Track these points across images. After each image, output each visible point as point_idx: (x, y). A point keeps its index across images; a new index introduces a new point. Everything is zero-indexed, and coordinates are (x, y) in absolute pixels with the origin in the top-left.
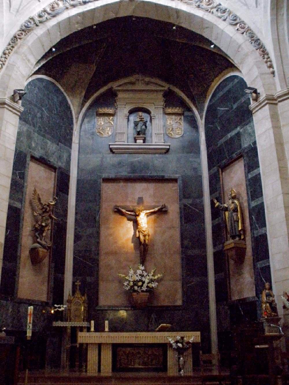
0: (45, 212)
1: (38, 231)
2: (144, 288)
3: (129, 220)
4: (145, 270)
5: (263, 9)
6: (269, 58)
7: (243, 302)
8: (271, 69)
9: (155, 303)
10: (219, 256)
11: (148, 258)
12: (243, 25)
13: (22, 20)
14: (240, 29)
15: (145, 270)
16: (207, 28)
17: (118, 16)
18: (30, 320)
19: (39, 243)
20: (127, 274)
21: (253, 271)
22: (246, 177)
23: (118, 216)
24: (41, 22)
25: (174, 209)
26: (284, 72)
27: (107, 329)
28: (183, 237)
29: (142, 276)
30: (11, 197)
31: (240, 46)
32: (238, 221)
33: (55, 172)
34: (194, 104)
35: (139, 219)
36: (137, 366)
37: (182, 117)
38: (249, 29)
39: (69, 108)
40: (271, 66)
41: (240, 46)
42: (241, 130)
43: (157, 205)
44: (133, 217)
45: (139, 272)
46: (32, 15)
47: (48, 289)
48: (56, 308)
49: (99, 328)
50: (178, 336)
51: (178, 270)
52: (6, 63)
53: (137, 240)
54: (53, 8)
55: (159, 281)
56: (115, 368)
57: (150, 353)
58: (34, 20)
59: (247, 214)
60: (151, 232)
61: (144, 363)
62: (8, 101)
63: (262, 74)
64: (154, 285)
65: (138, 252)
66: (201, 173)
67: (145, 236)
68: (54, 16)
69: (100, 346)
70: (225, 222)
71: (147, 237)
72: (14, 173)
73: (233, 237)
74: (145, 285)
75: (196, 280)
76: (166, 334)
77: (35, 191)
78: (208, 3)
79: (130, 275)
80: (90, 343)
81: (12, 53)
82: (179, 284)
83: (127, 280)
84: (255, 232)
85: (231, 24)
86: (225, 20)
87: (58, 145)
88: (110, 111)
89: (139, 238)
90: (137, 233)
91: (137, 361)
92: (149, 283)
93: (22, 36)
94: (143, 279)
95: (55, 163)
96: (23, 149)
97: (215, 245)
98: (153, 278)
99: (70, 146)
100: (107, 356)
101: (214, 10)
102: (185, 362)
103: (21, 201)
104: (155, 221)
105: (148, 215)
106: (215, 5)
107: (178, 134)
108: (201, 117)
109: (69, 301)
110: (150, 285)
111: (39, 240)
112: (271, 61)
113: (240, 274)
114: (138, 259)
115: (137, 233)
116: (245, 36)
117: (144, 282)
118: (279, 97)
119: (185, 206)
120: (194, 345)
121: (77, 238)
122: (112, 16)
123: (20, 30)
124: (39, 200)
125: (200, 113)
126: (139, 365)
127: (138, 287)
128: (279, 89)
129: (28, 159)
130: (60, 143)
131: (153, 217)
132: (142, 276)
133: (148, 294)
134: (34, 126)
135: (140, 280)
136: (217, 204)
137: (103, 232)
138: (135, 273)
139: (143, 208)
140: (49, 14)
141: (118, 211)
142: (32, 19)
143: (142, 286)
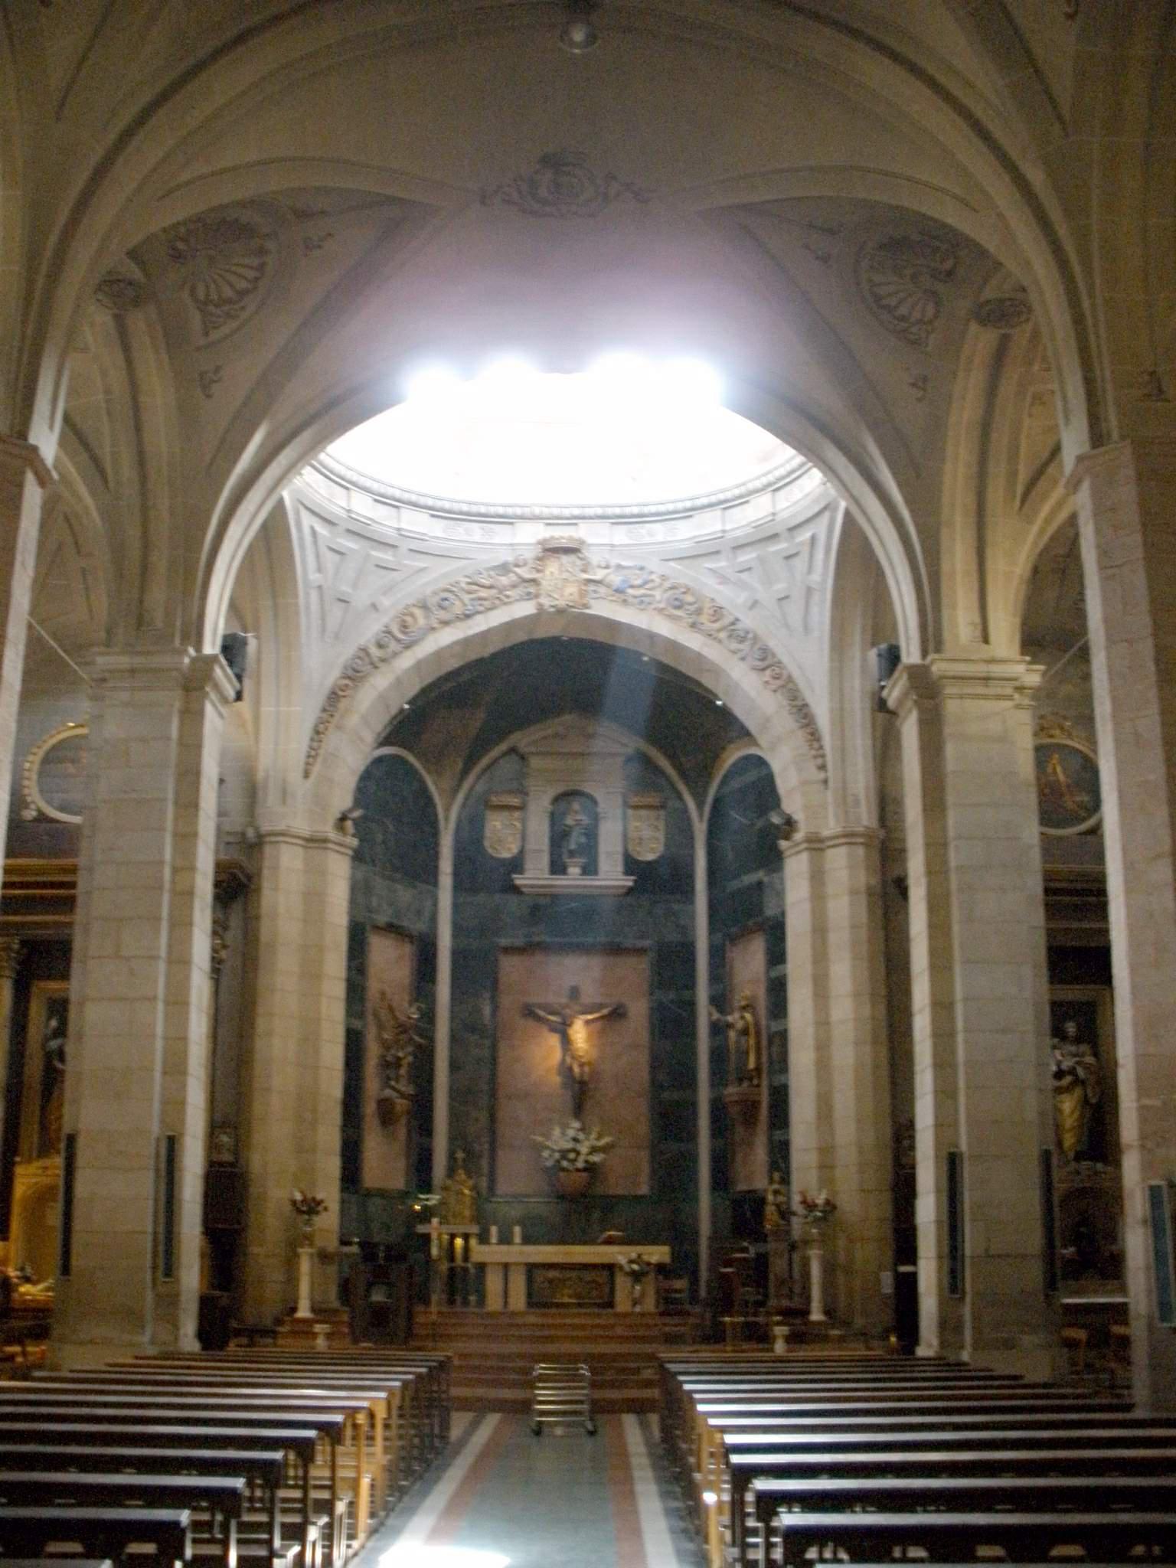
0: (405, 1032)
1: (389, 1066)
2: (580, 1164)
3: (553, 1030)
4: (582, 1130)
9: (600, 1190)
13: (347, 652)
14: (772, 681)
15: (582, 1130)
16: (708, 671)
18: (706, 1351)
20: (547, 1135)
23: (531, 1023)
24: (383, 660)
25: (639, 1009)
29: (575, 1140)
31: (768, 720)
32: (747, 1053)
33: (412, 942)
34: (687, 782)
36: (566, 1300)
40: (822, 767)
41: (768, 720)
42: (766, 879)
43: (608, 1001)
44: (559, 1027)
45: (571, 1133)
46: (362, 642)
49: (505, 1239)
50: (633, 1251)
51: (643, 1129)
52: (321, 752)
53: (566, 1071)
54: (404, 627)
56: (531, 1304)
59: (764, 1043)
61: (578, 1296)
63: (805, 783)
64: (596, 1158)
67: (582, 1065)
68: (408, 647)
69: (506, 1267)
74: (581, 1158)
78: (715, 618)
79: (554, 1138)
80: (491, 1263)
81: (331, 727)
82: (644, 1155)
83: (548, 1148)
85: (754, 669)
86: (743, 659)
87: (415, 887)
88: (515, 801)
89: (570, 1069)
92: (588, 1155)
94: (579, 1147)
97: (713, 1085)
100: (518, 1284)
101: (723, 635)
103: (361, 1015)
104: (602, 1033)
105: (587, 1022)
107: (652, 850)
108: (701, 816)
111: (393, 1083)
112: (823, 756)
113: (750, 1145)
120: (661, 1268)
121: (454, 1066)
122: (521, 637)
125: (700, 805)
128: (832, 822)
129: (368, 928)
132: (575, 1140)
135: (574, 1150)
136: (716, 1016)
137: (504, 1053)
138: (563, 1134)
141: (529, 1012)
142: (364, 650)
143: (575, 1160)
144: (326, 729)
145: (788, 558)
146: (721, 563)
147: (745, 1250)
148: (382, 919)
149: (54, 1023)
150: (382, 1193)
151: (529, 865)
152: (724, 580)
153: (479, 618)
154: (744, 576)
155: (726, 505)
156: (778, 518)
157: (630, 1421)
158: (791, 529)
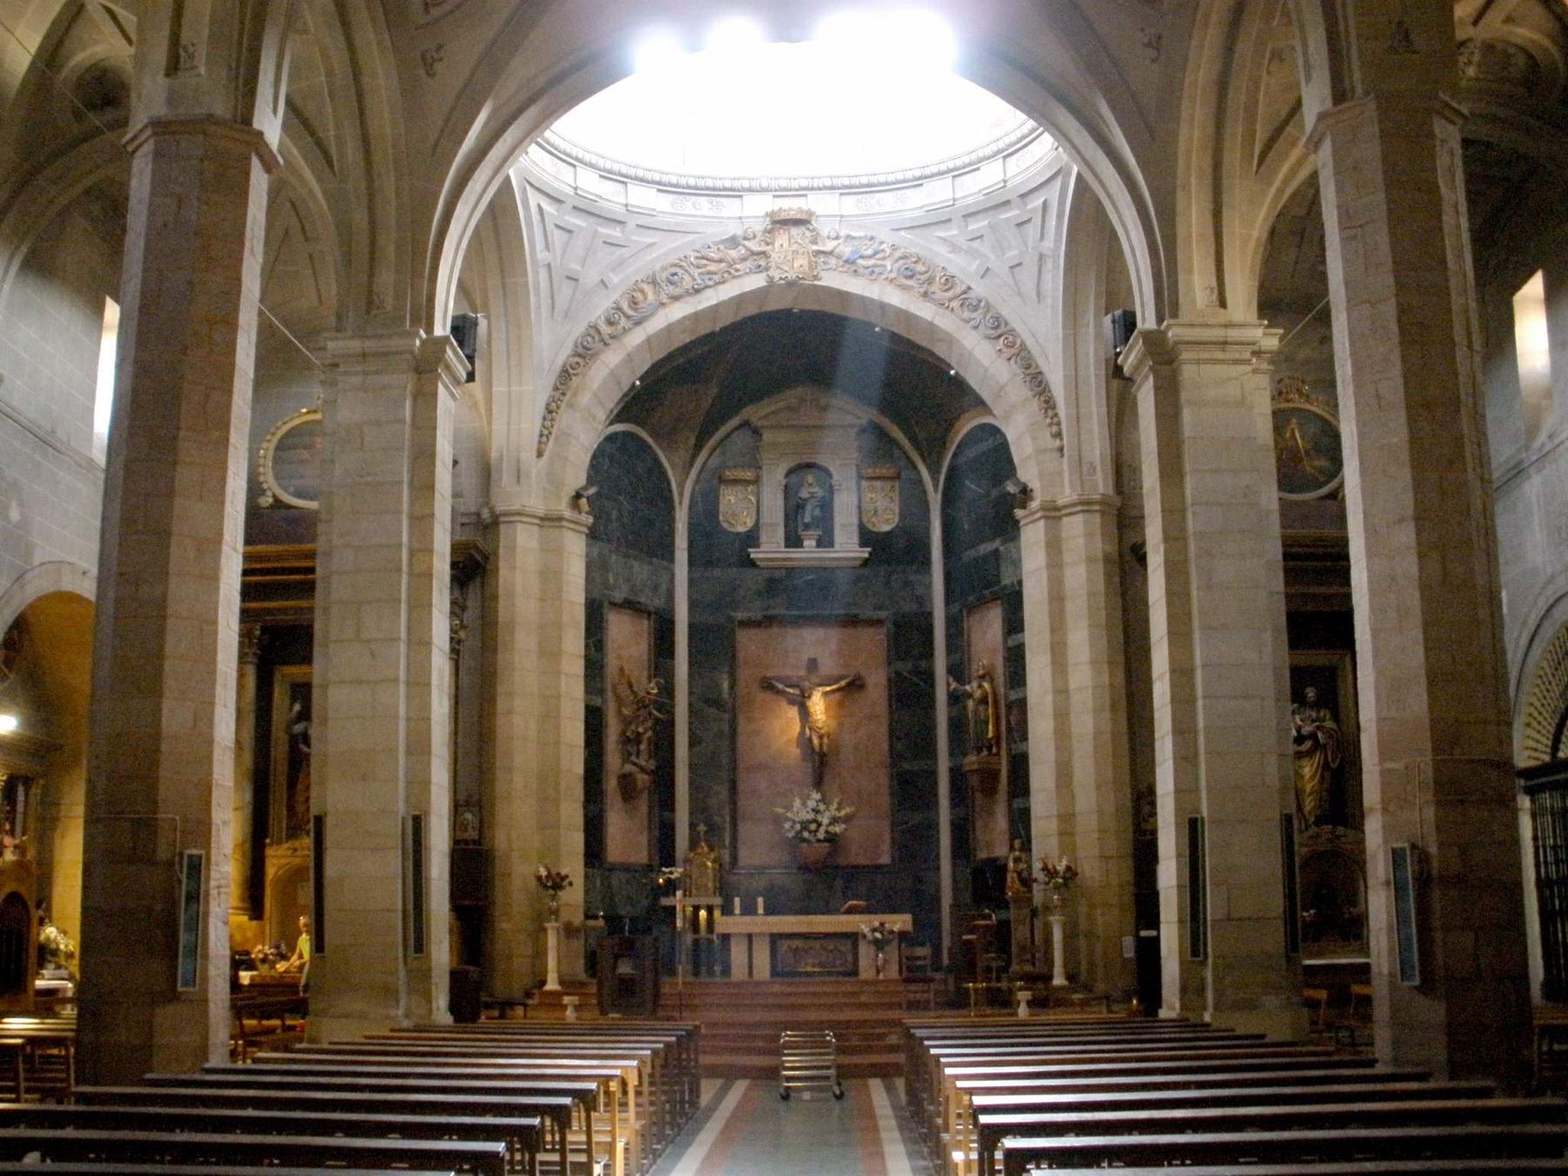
1: (629, 742)
2: (821, 835)
3: (792, 702)
5: (1049, 310)
6: (1056, 415)
7: (992, 861)
8: (1058, 443)
9: (842, 861)
10: (957, 774)
11: (827, 778)
12: (1011, 338)
14: (1005, 350)
17: (763, 310)
19: (635, 764)
20: (789, 808)
21: (1108, 715)
22: (1005, 640)
23: (768, 696)
24: (613, 337)
25: (877, 681)
26: (1079, 451)
27: (761, 911)
28: (892, 734)
29: (816, 811)
30: (588, 691)
32: (987, 723)
33: (649, 618)
35: (809, 703)
36: (809, 969)
37: (897, 484)
38: (1023, 347)
39: (663, 474)
40: (1058, 435)
42: (1001, 548)
45: (811, 804)
47: (649, 841)
48: (665, 873)
49: (749, 910)
50: (876, 920)
51: (885, 800)
52: (554, 431)
53: (805, 742)
54: (634, 303)
55: (847, 819)
56: (774, 973)
57: (831, 947)
58: (599, 332)
60: (833, 724)
61: (821, 965)
62: (568, 513)
63: (1040, 452)
64: (837, 829)
65: (810, 765)
66: (932, 607)
67: (821, 737)
68: (638, 323)
69: (750, 937)
70: (966, 716)
71: (825, 740)
72: (587, 646)
73: (979, 750)
74: (822, 829)
75: (916, 818)
76: (856, 918)
77: (622, 669)
79: (795, 809)
81: (563, 406)
82: (885, 825)
84: (1013, 746)
85: (988, 337)
86: (976, 328)
87: (651, 563)
89: (810, 740)
90: (807, 731)
91: (810, 961)
92: (830, 824)
93: (579, 370)
94: (819, 818)
95: (649, 602)
96: (596, 594)
97: (951, 754)
98: (838, 814)
99: (672, 560)
102: (885, 960)
103: (601, 692)
104: (841, 705)
105: (826, 694)
106: (958, 290)
108: (936, 486)
109: (687, 861)
110: (831, 829)
112: (1059, 424)
113: (991, 813)
114: (809, 779)
115: (807, 731)
116: (1014, 366)
117: (820, 825)
118: (1066, 507)
119: (898, 674)
120: (903, 936)
122: (752, 310)
123: (574, 355)
124: (630, 686)
125: (934, 473)
126: (814, 966)
127: (810, 832)
129: (606, 604)
130: (654, 560)
131: (837, 695)
132: (816, 811)
133: (826, 844)
134: (609, 541)
135: (815, 821)
136: (954, 685)
138: (804, 804)
139: (817, 680)
140: (628, 317)
141: (768, 685)
143: (817, 831)
144: (558, 407)
145: (1019, 225)
146: (951, 232)
147: (988, 917)
148: (619, 596)
149: (297, 707)
150: (626, 868)
151: (763, 538)
152: (955, 248)
153: (709, 292)
154: (976, 244)
155: (956, 172)
156: (1009, 185)
157: (876, 1086)
158: (1023, 196)
